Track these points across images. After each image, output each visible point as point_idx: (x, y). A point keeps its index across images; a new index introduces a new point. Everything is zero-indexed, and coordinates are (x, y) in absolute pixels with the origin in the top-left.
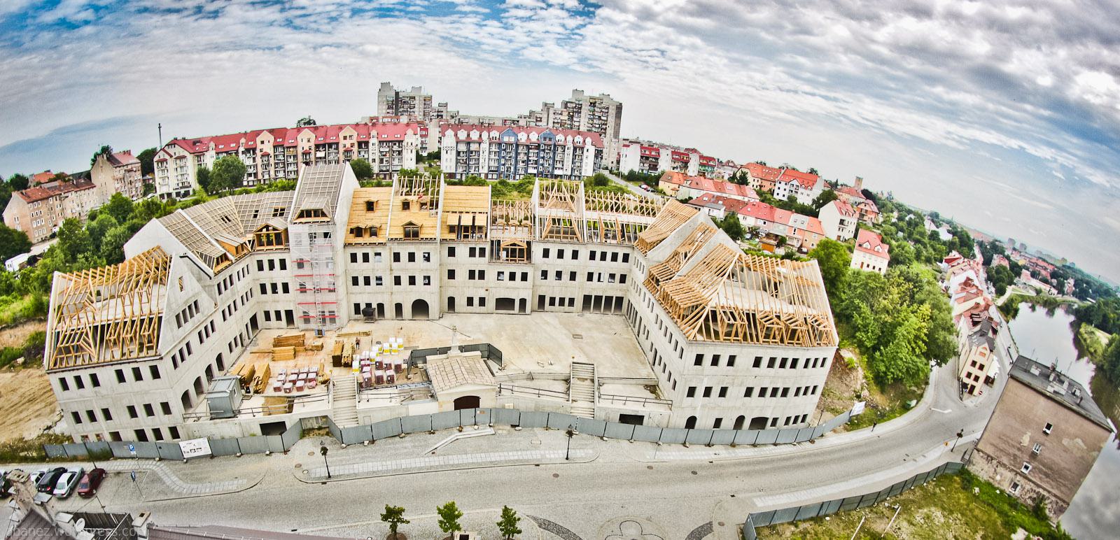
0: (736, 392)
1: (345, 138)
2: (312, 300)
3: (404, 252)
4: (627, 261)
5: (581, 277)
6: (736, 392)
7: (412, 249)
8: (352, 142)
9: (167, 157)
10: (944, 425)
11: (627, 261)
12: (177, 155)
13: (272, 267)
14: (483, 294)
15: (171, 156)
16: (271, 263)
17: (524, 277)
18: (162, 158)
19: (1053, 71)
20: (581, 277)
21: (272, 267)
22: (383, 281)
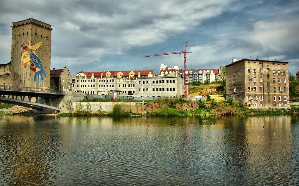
0: (150, 90)
1: (131, 74)
2: (92, 104)
3: (155, 80)
4: (174, 83)
6: (150, 90)
7: (144, 80)
8: (133, 76)
9: (79, 76)
10: (27, 116)
11: (174, 83)
12: (83, 76)
13: (131, 86)
14: (126, 90)
15: (81, 76)
16: (131, 85)
17: (174, 82)
18: (78, 76)
19: (265, 124)
21: (131, 86)
22: (124, 84)
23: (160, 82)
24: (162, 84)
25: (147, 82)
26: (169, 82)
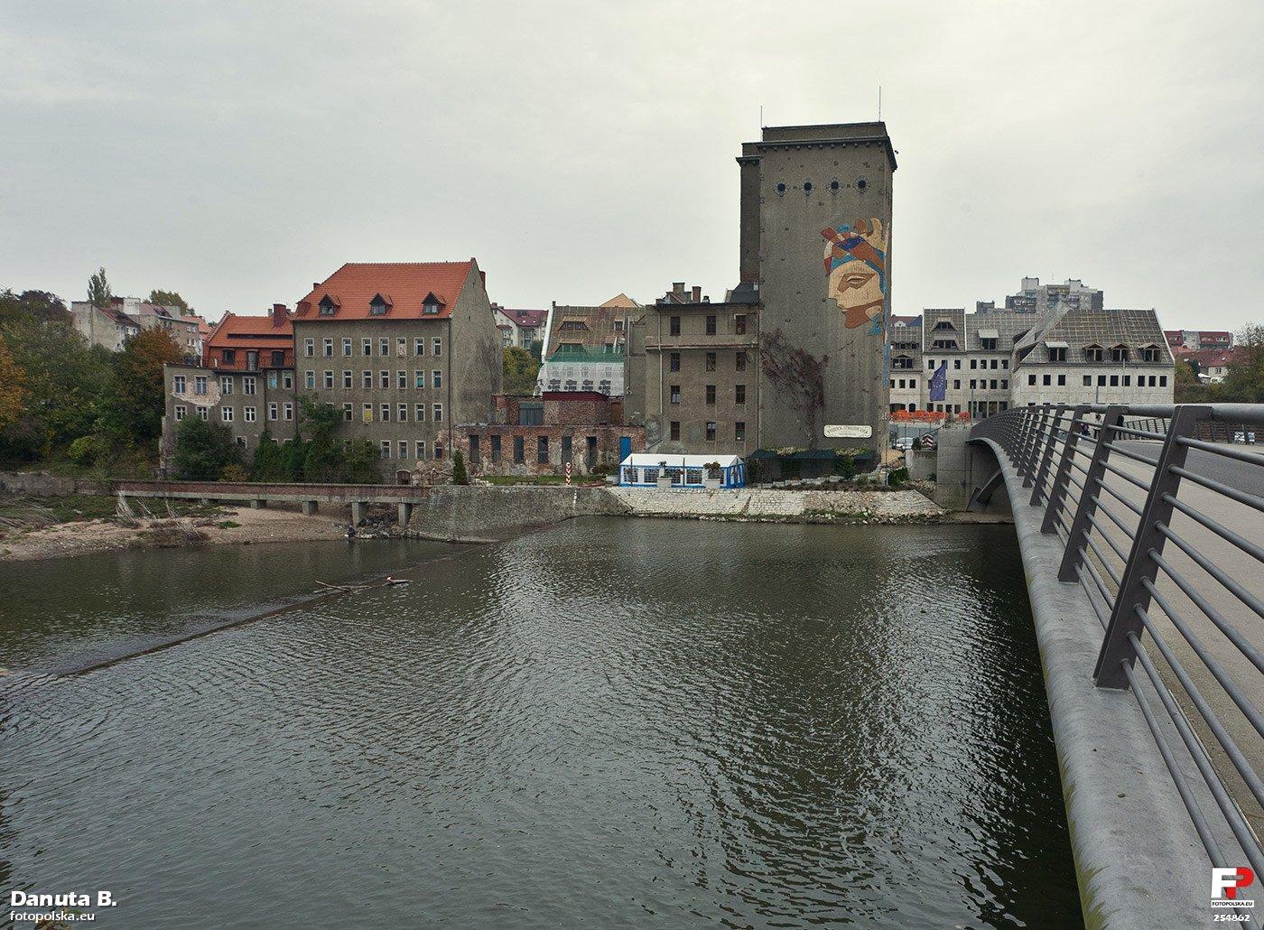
5: (965, 386)
16: (984, 362)
20: (965, 386)
23: (1114, 381)
24: (1120, 388)
25: (1062, 380)
26: (1147, 381)
